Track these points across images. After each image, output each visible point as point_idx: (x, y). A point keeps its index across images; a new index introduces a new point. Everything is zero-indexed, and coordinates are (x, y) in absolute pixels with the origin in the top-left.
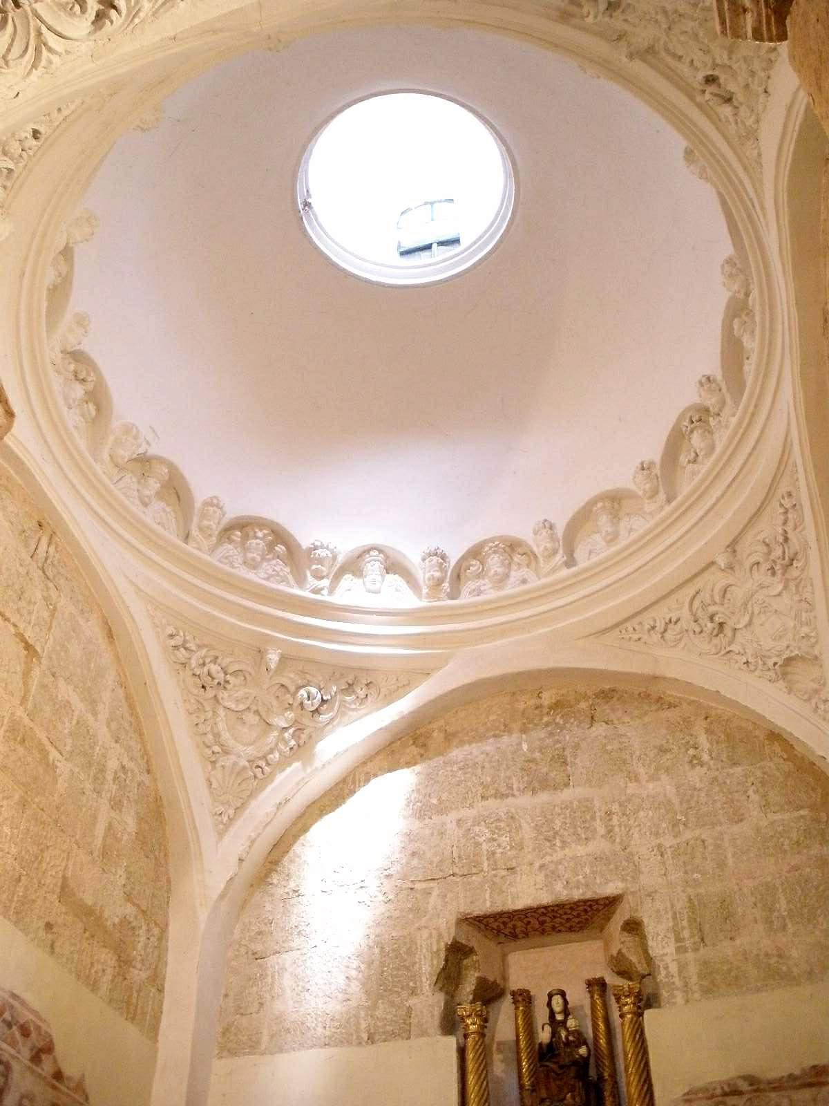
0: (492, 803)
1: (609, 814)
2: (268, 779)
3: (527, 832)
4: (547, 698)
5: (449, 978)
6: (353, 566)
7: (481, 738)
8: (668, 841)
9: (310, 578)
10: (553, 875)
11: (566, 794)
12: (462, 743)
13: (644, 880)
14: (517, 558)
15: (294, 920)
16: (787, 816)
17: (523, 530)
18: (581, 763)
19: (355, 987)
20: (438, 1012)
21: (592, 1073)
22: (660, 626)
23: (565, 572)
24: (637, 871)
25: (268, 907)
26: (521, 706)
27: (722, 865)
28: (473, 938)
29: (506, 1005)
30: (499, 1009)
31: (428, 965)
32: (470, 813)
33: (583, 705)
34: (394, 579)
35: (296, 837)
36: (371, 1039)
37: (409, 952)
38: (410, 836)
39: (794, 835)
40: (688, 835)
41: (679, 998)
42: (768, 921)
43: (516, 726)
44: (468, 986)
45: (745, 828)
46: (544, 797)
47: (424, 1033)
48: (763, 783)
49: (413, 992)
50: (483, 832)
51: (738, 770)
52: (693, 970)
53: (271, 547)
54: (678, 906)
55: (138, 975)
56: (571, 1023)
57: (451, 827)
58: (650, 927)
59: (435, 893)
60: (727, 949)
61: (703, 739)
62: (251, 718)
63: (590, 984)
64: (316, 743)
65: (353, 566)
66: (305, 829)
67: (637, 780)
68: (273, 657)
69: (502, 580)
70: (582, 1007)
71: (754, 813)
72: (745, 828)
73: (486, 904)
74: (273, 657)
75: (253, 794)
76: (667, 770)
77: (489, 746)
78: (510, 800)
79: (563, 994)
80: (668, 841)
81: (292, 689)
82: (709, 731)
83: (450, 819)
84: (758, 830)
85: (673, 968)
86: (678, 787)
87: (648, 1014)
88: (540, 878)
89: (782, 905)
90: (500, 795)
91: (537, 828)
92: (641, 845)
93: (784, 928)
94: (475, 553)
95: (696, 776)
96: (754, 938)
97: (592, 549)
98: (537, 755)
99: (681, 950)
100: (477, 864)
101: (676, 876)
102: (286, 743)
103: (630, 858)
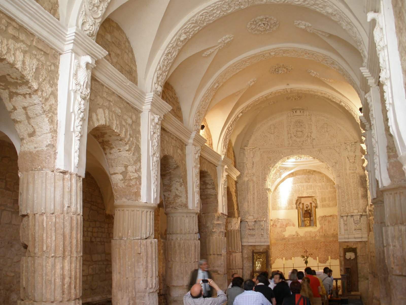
3: (305, 188)
5: (296, 203)
8: (320, 191)
10: (308, 193)
11: (309, 184)
31: (294, 202)
40: (322, 190)
44: (298, 203)
46: (307, 183)
51: (328, 183)
52: (321, 205)
71: (329, 189)
73: (300, 196)
77: (301, 176)
80: (320, 191)
83: (296, 185)
90: (302, 183)
95: (323, 183)
96: (327, 202)
101: (320, 195)
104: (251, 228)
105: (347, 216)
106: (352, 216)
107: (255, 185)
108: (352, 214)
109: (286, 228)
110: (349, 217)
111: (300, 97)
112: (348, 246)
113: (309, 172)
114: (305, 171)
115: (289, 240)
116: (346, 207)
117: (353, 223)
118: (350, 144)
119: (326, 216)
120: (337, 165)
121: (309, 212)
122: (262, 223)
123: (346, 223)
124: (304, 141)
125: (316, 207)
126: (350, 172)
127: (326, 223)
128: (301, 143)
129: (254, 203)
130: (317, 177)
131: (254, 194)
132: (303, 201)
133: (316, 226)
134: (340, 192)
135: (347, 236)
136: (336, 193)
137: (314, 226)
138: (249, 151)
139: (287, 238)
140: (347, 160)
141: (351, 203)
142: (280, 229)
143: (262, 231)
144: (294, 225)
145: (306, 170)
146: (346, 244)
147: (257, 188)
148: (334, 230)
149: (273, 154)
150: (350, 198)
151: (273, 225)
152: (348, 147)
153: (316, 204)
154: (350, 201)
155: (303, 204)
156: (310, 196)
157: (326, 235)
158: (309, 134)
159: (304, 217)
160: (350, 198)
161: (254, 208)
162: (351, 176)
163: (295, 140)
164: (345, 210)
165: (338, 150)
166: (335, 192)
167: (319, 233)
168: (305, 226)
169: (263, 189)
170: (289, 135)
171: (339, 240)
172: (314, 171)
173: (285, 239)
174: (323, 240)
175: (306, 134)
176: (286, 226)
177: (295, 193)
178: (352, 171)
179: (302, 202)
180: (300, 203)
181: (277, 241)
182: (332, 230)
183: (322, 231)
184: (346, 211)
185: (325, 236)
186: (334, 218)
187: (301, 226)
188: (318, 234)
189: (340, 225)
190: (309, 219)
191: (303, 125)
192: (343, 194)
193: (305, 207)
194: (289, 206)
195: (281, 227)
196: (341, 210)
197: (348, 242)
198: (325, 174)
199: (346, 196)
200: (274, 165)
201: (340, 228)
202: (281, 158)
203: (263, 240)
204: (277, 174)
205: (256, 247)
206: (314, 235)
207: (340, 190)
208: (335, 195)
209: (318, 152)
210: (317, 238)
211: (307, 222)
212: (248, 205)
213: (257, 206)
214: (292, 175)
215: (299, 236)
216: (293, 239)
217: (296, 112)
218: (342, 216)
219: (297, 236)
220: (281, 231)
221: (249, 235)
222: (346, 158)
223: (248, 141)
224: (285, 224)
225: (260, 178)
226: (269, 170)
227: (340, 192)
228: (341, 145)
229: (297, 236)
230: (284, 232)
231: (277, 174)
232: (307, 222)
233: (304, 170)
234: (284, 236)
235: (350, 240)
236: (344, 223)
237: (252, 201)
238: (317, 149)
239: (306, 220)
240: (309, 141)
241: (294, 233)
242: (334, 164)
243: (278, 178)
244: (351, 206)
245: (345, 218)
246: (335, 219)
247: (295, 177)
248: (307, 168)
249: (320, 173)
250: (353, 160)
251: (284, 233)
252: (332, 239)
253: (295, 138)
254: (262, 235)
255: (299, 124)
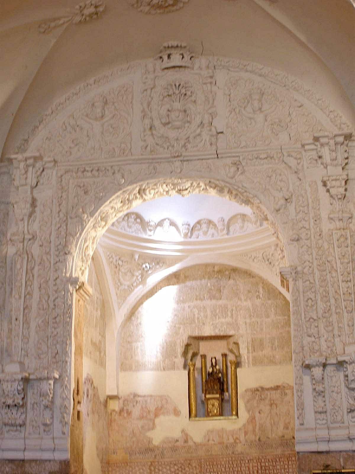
0: (199, 302)
1: (232, 310)
2: (132, 291)
3: (209, 313)
4: (216, 269)
5: (185, 353)
6: (160, 224)
7: (195, 279)
8: (248, 321)
9: (148, 231)
10: (215, 327)
11: (220, 302)
12: (190, 280)
13: (241, 332)
14: (211, 225)
15: (140, 333)
16: (280, 318)
17: (215, 219)
18: (225, 292)
19: (159, 355)
20: (183, 363)
21: (222, 380)
22: (253, 257)
23: (226, 236)
24: (239, 328)
25: (132, 327)
26: (208, 270)
27: (262, 329)
28: (192, 342)
29: (199, 358)
30: (197, 358)
31: (180, 350)
32: (192, 304)
33: (227, 273)
34: (173, 228)
35: (139, 306)
36: (164, 369)
37: (175, 346)
38: (175, 310)
39: (282, 324)
40: (253, 320)
41: (246, 365)
42: (272, 347)
43: (207, 277)
44: (190, 355)
45: (269, 320)
46: (214, 302)
47: (178, 369)
48: (276, 307)
49: (176, 357)
50: (196, 311)
51: (270, 302)
53: (135, 220)
54: (249, 340)
55: (102, 354)
56: (217, 367)
57: (187, 308)
58: (241, 346)
59: (182, 328)
60: (260, 353)
61: (261, 290)
62: (129, 274)
63: (222, 355)
64: (147, 279)
65: (160, 224)
66: (142, 303)
67: (241, 300)
68: (137, 257)
69: (205, 233)
70: (220, 360)
71: (272, 316)
72: (269, 320)
73: (196, 334)
74: (137, 257)
75: (129, 295)
76: (250, 299)
77: (198, 282)
78: (204, 301)
79: (215, 358)
80: (248, 321)
81: (141, 264)
82: (263, 288)
83: (186, 305)
84: (273, 321)
85: (246, 357)
86: (252, 305)
87: (238, 370)
88: (212, 327)
89: (276, 344)
90: (201, 299)
91: (212, 312)
92: (241, 321)
93: (276, 349)
94: (199, 222)
95: (258, 302)
96: (267, 351)
97: (235, 227)
98: (213, 288)
99: (248, 352)
100: (194, 321)
101: (249, 331)
102: (138, 280)
103: (237, 324)
104: (10, 402)
105: (324, 365)
106: (341, 364)
107: (36, 268)
108: (340, 359)
109: (157, 421)
110: (329, 369)
111: (250, 274)
112: (327, 467)
113: (219, 272)
114: (209, 269)
115: (162, 453)
116: (319, 338)
117: (344, 390)
118: (332, 142)
119: (262, 388)
120: (292, 208)
121: (219, 379)
122: (48, 386)
123: (320, 388)
124: (191, 139)
125: (238, 364)
126: (332, 226)
127: (266, 409)
128: (182, 142)
129: (26, 322)
130: (242, 284)
131: (29, 294)
132: (204, 348)
133: (237, 414)
134: (301, 290)
135: (323, 433)
136: (290, 326)
137: (232, 415)
138: (22, 165)
139: (158, 448)
140: (322, 190)
141: (336, 325)
142: (140, 423)
143: (47, 414)
144: (177, 413)
145: (214, 265)
146: (323, 460)
147: (39, 276)
148: (286, 427)
149: (94, 176)
150: (333, 308)
151: (121, 411)
152: (326, 152)
153: (238, 356)
154: (334, 318)
155: (204, 357)
156: (222, 334)
157: (263, 439)
158: (206, 116)
159: (206, 391)
160: (333, 308)
161: (26, 339)
162: (335, 237)
163: (162, 136)
164: (316, 348)
165: (292, 162)
166: (288, 323)
167: (246, 433)
168: (208, 414)
169: (58, 281)
170: (147, 121)
171: (299, 448)
172: (235, 270)
173: (152, 450)
174: (254, 453)
175: (198, 120)
176: (156, 416)
177: (182, 326)
178: (339, 224)
179: (201, 353)
180: (195, 355)
181: (130, 455)
182: (281, 426)
183: (254, 431)
184: (319, 350)
185: (261, 444)
186: (286, 394)
187: (196, 416)
188: (242, 438)
189: (300, 397)
190: (218, 396)
191: (189, 93)
192: (312, 296)
193: (209, 365)
194: (164, 361)
195: (141, 417)
196: (303, 348)
197: (328, 452)
198: (261, 278)
199: (319, 302)
200: (96, 210)
201: (303, 404)
202: (119, 187)
203: (47, 443)
204: (133, 275)
205: (27, 465)
206: (231, 440)
207: (300, 283)
208: (289, 332)
209: (233, 169)
210: (239, 448)
211: (214, 405)
212: (10, 330)
213: (37, 332)
214: (175, 280)
215: (190, 443)
216: (174, 449)
217: (169, 56)
218: (308, 367)
219: (186, 441)
220: (142, 427)
221: (6, 425)
222: (320, 184)
223: (26, 141)
224: (153, 409)
225: (52, 245)
226: (82, 224)
227: (301, 290)
228: (303, 146)
229: (186, 441)
230: (149, 430)
231: (133, 275)
232: (213, 405)
233: (207, 265)
234: (150, 441)
235: (333, 447)
236: (314, 389)
237: (21, 318)
238: (229, 161)
239: (209, 399)
240: (205, 136)
241: (177, 434)
242: (283, 202)
243: (137, 285)
244: (336, 332)
245: (317, 372)
246: (288, 398)
247: (182, 285)
248: (213, 261)
249: (248, 274)
250: (342, 190)
251: (149, 434)
252: (279, 451)
253: (162, 130)
254: (45, 425)
255: (177, 92)
